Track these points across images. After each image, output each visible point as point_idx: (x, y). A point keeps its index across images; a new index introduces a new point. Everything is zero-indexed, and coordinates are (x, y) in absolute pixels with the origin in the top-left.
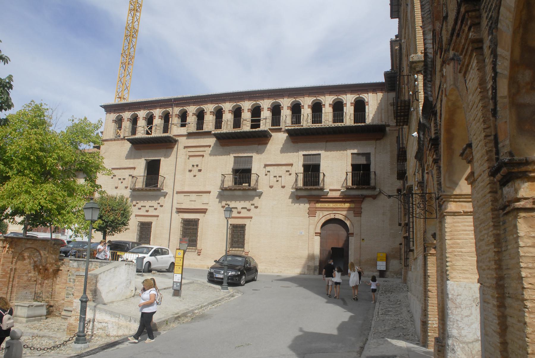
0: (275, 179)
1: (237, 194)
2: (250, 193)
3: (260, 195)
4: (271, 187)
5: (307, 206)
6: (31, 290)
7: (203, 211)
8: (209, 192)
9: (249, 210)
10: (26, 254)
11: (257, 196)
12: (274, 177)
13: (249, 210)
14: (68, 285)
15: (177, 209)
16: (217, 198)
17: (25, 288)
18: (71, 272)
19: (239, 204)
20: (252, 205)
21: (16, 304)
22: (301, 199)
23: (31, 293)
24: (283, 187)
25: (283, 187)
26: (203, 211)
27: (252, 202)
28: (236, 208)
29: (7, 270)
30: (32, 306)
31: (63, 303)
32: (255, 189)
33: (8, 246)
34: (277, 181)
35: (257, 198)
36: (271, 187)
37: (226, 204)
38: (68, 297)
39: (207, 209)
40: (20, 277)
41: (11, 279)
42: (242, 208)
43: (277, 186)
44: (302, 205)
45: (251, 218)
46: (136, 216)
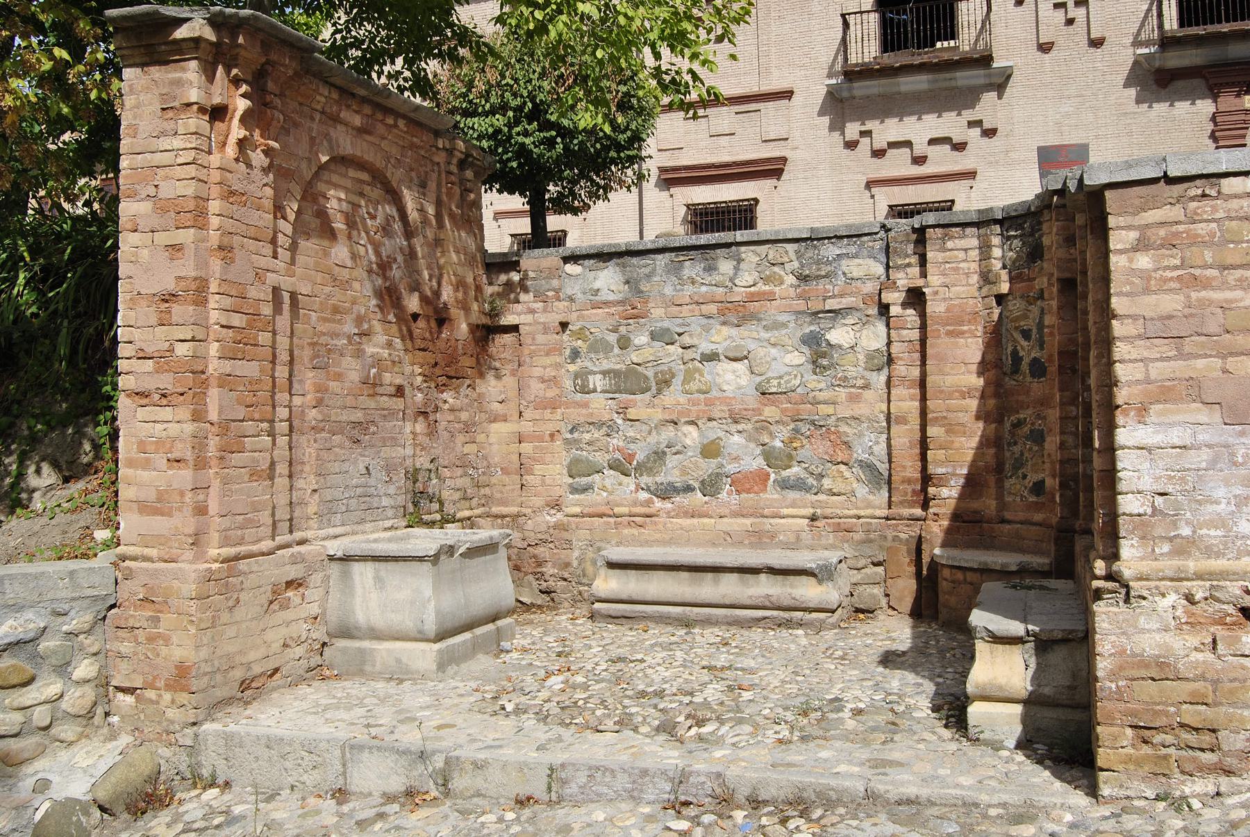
0: (1060, 15)
1: (903, 88)
2: (965, 78)
3: (1000, 83)
4: (1045, 48)
5: (1206, 107)
6: (387, 452)
7: (772, 169)
8: (788, 94)
9: (959, 147)
10: (335, 202)
11: (989, 87)
12: (1056, 6)
13: (959, 147)
14: (577, 415)
15: (662, 170)
16: (821, 113)
17: (358, 433)
18: (580, 334)
19: (919, 125)
20: (971, 124)
21: (335, 548)
22: (1180, 84)
23: (389, 469)
24: (1096, 43)
25: (1096, 43)
26: (772, 169)
27: (969, 115)
28: (908, 144)
29: (253, 293)
30: (450, 550)
31: (560, 527)
32: (985, 60)
33: (242, 105)
34: (1070, 22)
35: (989, 97)
36: (1045, 48)
37: (863, 134)
38: (585, 489)
39: (784, 160)
40: (323, 358)
41: (282, 372)
42: (932, 142)
43: (1071, 43)
44: (1182, 107)
45: (972, 175)
46: (498, 216)
